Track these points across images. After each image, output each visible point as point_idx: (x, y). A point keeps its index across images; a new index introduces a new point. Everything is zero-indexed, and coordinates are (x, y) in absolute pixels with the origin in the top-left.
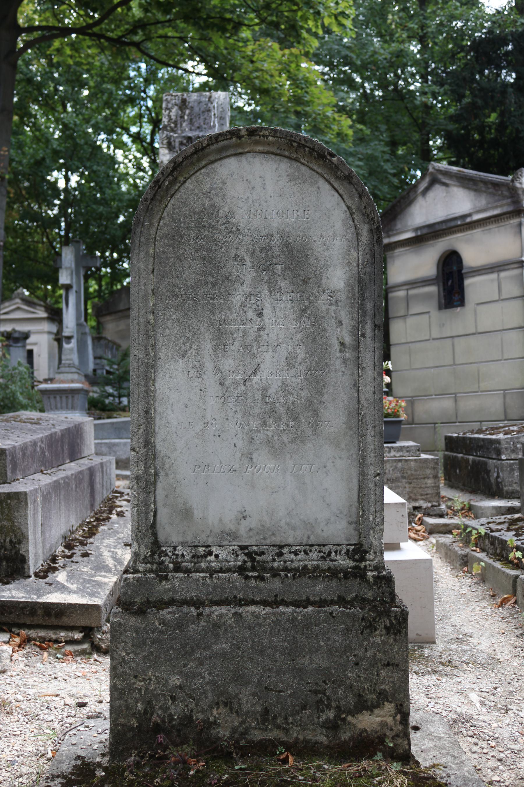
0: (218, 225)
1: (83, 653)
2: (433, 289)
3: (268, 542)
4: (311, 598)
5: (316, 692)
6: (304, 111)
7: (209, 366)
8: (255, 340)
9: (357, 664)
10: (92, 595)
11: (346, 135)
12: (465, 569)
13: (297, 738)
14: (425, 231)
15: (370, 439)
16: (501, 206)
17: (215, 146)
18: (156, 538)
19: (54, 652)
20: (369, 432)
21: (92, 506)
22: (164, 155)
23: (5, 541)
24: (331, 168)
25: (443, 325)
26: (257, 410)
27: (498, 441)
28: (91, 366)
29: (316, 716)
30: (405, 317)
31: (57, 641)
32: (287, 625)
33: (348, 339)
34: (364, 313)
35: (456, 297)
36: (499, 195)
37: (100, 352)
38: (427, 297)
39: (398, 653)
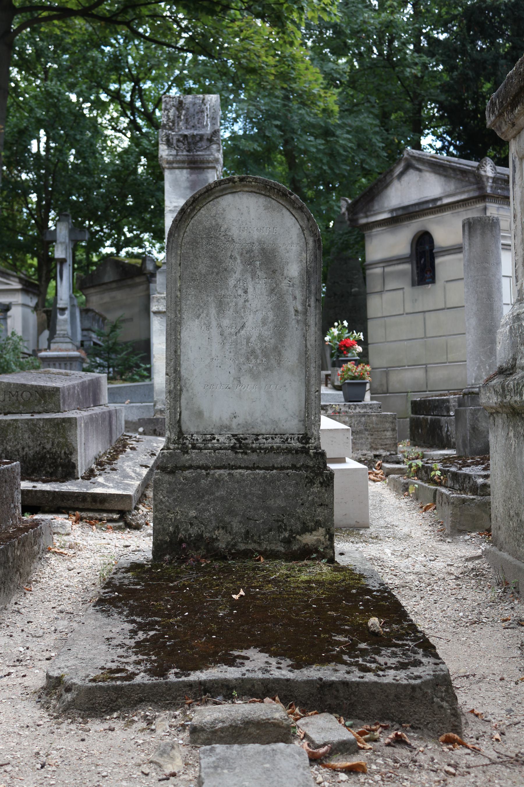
0: (220, 237)
1: (119, 528)
2: (407, 267)
3: (249, 432)
4: (276, 466)
5: (278, 521)
6: (291, 87)
7: (214, 323)
8: (243, 308)
9: (302, 504)
10: (125, 489)
11: (332, 111)
12: (406, 493)
13: (266, 549)
14: (400, 213)
15: (313, 369)
16: (468, 191)
17: (219, 188)
18: (181, 429)
19: (99, 526)
20: (312, 365)
21: (111, 441)
22: (163, 150)
23: (61, 453)
24: (290, 202)
25: (416, 300)
26: (243, 351)
27: (448, 401)
28: (79, 338)
29: (277, 535)
30: (381, 292)
31: (101, 520)
32: (261, 481)
33: (300, 308)
34: (310, 292)
35: (428, 275)
36: (466, 181)
37: (87, 325)
38: (401, 274)
39: (327, 498)
